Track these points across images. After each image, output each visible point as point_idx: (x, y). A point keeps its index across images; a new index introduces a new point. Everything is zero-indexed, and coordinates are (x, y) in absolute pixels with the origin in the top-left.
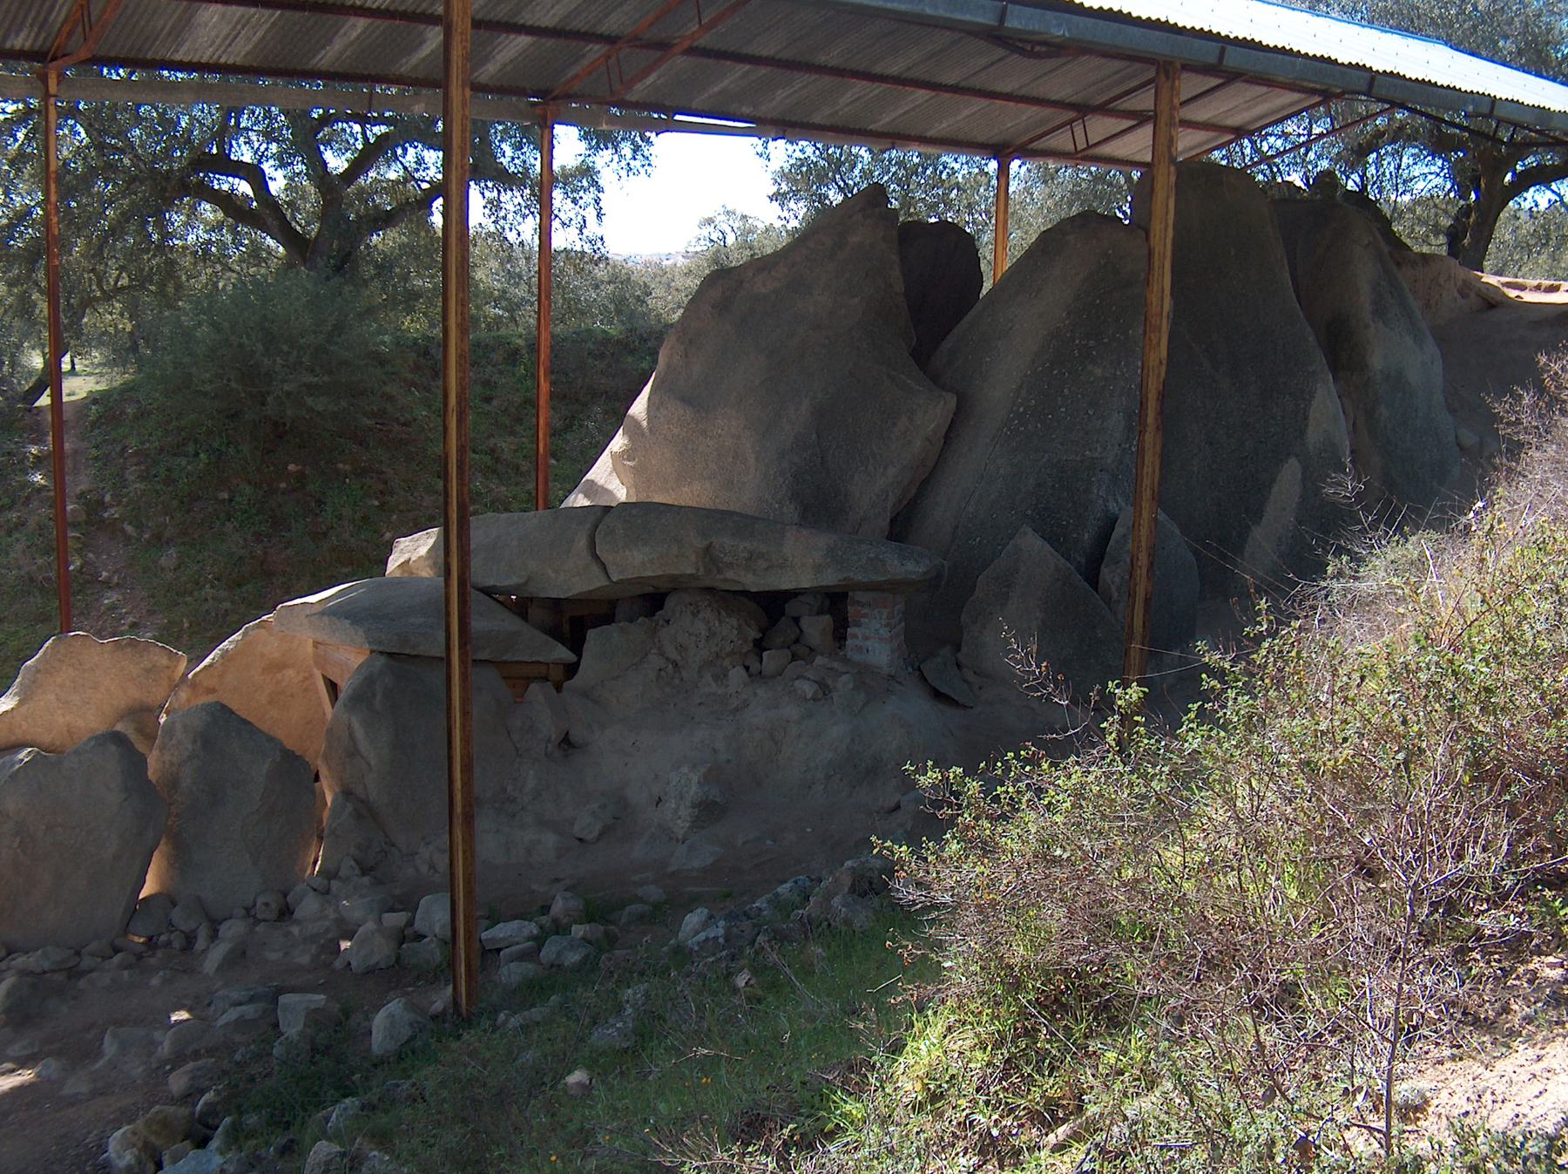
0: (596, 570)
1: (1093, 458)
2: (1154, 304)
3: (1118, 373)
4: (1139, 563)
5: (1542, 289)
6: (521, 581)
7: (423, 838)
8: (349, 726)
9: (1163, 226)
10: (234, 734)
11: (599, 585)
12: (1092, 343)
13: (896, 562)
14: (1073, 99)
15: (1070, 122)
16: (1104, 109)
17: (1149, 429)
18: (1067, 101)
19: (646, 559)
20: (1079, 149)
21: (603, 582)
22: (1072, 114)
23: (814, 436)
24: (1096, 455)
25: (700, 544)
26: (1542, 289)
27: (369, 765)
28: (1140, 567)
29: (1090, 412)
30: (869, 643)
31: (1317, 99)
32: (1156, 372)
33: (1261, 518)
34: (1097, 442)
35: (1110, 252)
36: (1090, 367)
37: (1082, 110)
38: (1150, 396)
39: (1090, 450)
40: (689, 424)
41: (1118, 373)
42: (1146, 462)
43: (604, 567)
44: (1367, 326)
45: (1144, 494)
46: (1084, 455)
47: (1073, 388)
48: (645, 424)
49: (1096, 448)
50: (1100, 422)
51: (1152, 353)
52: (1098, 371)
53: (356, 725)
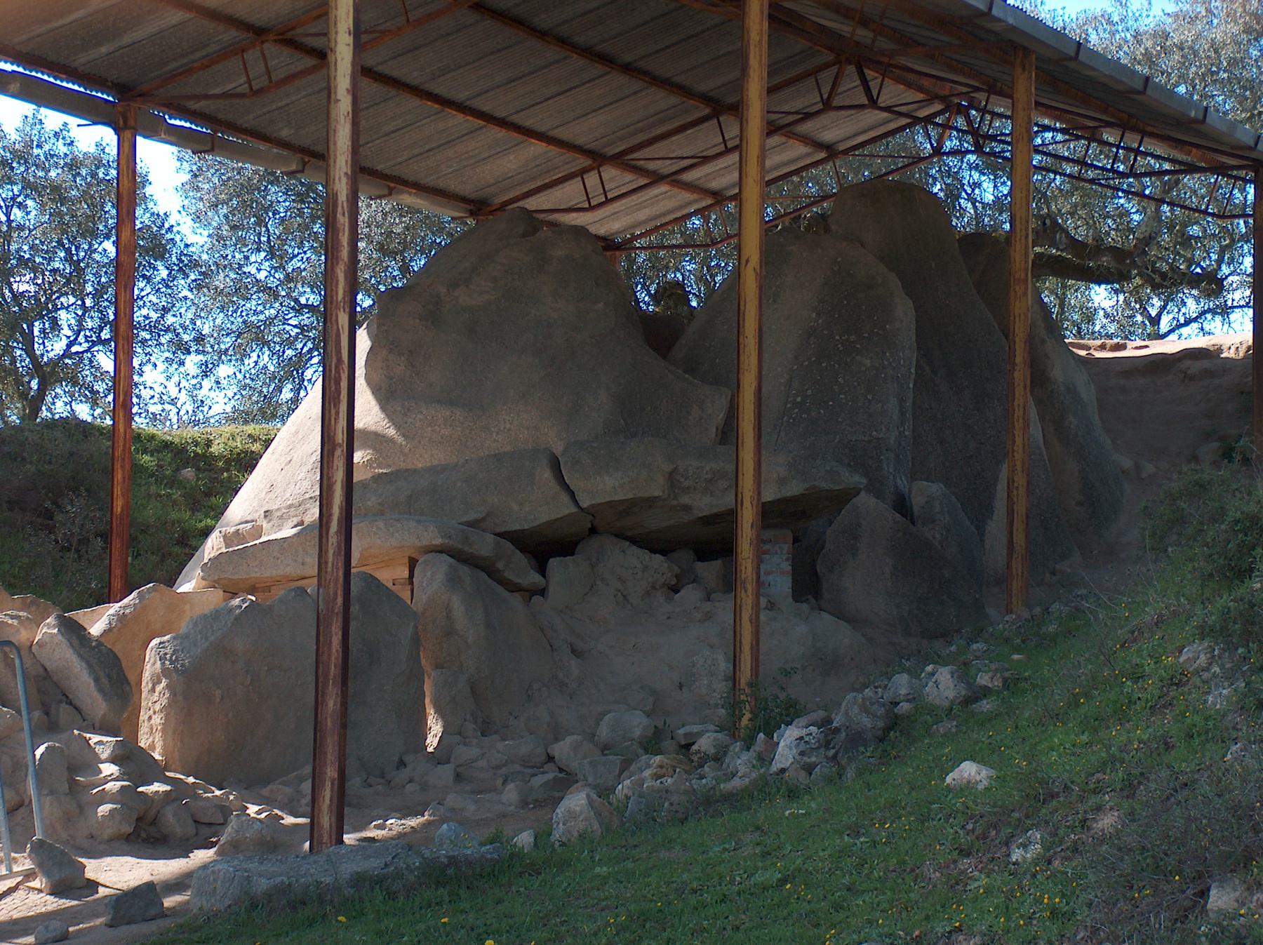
0: (565, 497)
1: (878, 439)
2: (1017, 260)
3: (886, 363)
4: (1016, 485)
5: (1108, 347)
6: (480, 516)
7: (511, 714)
8: (448, 609)
9: (1024, 194)
10: (384, 599)
11: (566, 512)
12: (852, 338)
13: (847, 474)
14: (592, 146)
15: (582, 173)
16: (620, 160)
17: (1017, 368)
18: (586, 147)
19: (617, 484)
20: (609, 198)
21: (567, 508)
22: (583, 162)
23: (622, 422)
24: (881, 436)
25: (667, 467)
26: (1108, 347)
27: (466, 642)
28: (1017, 488)
29: (870, 397)
30: (771, 577)
31: (823, 155)
32: (1023, 317)
33: (992, 514)
34: (881, 423)
35: (839, 259)
36: (858, 358)
37: (598, 159)
38: (1017, 339)
39: (876, 431)
40: (463, 423)
41: (886, 363)
42: (1017, 396)
43: (572, 494)
44: (1043, 342)
45: (1016, 424)
46: (871, 435)
47: (847, 378)
48: (392, 432)
49: (881, 429)
50: (879, 405)
51: (1017, 303)
52: (868, 362)
53: (457, 605)
